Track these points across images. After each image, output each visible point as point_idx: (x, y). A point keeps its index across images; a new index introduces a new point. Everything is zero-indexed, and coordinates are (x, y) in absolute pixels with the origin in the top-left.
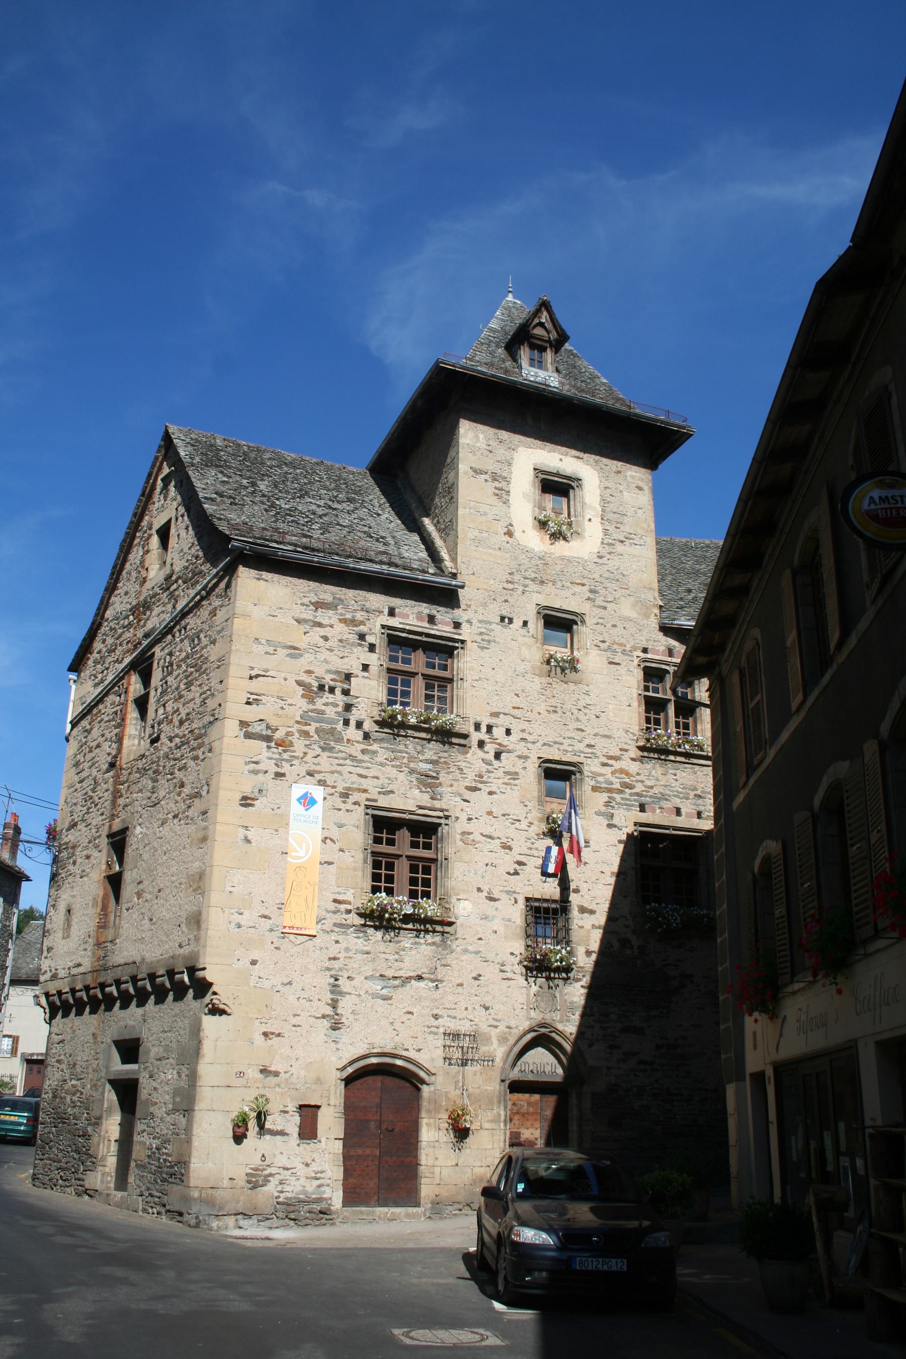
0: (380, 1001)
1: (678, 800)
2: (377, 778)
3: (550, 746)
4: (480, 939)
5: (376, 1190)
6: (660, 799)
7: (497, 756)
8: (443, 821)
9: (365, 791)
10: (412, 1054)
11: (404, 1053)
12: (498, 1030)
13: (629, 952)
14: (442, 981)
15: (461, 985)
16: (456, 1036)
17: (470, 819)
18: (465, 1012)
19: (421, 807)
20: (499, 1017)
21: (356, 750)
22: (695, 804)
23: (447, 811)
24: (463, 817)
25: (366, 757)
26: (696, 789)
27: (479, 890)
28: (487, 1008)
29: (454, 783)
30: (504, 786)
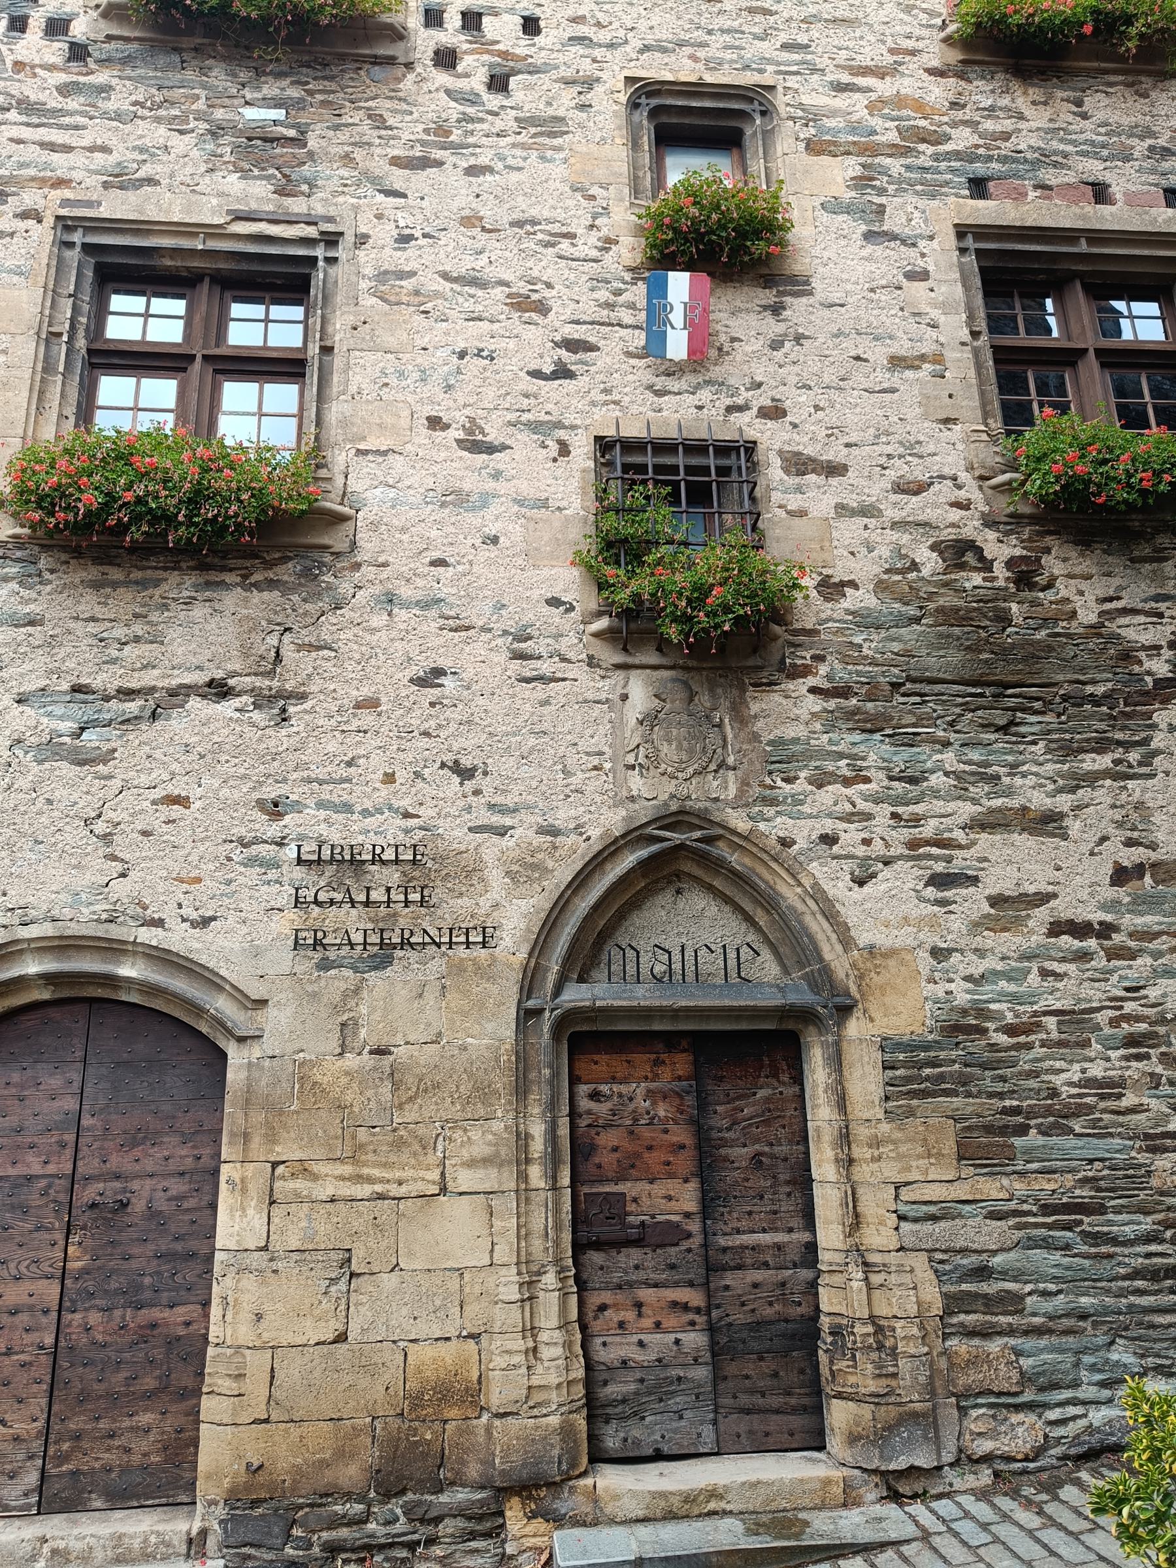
0: (66, 769)
1: (1098, 165)
2: (105, 149)
3: (664, 50)
4: (440, 563)
5: (37, 1445)
6: (1035, 164)
7: (498, 83)
8: (319, 252)
9: (60, 183)
10: (178, 938)
11: (147, 935)
12: (507, 842)
13: (977, 579)
14: (303, 697)
15: (371, 704)
16: (352, 863)
17: (405, 239)
18: (385, 791)
19: (239, 217)
20: (509, 800)
21: (41, 89)
22: (1153, 171)
23: (330, 219)
24: (383, 234)
25: (72, 104)
26: (1153, 135)
27: (435, 423)
28: (465, 774)
29: (359, 154)
30: (518, 152)
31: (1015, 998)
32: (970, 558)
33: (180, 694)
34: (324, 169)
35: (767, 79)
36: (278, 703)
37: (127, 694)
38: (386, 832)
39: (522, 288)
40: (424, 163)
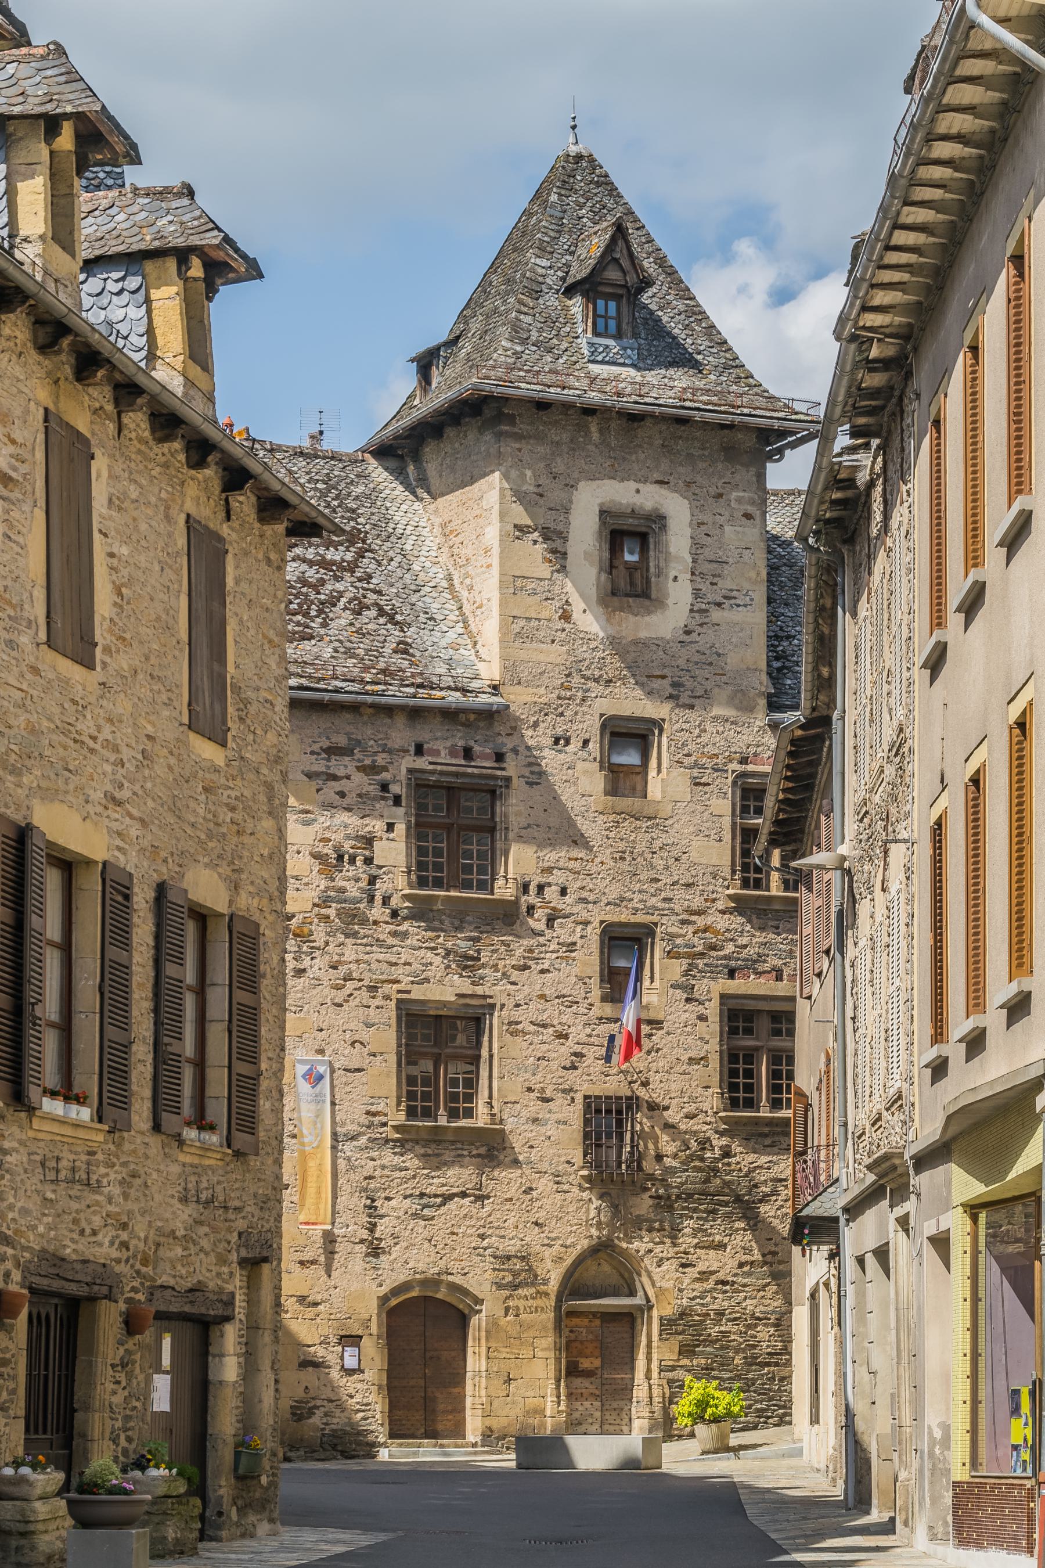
4: (532, 1147)
11: (450, 1278)
24: (510, 1003)
31: (703, 1305)
32: (707, 1145)
33: (451, 1197)
34: (486, 971)
35: (655, 918)
36: (481, 1198)
37: (436, 1196)
38: (511, 1247)
39: (559, 1028)
40: (525, 968)
